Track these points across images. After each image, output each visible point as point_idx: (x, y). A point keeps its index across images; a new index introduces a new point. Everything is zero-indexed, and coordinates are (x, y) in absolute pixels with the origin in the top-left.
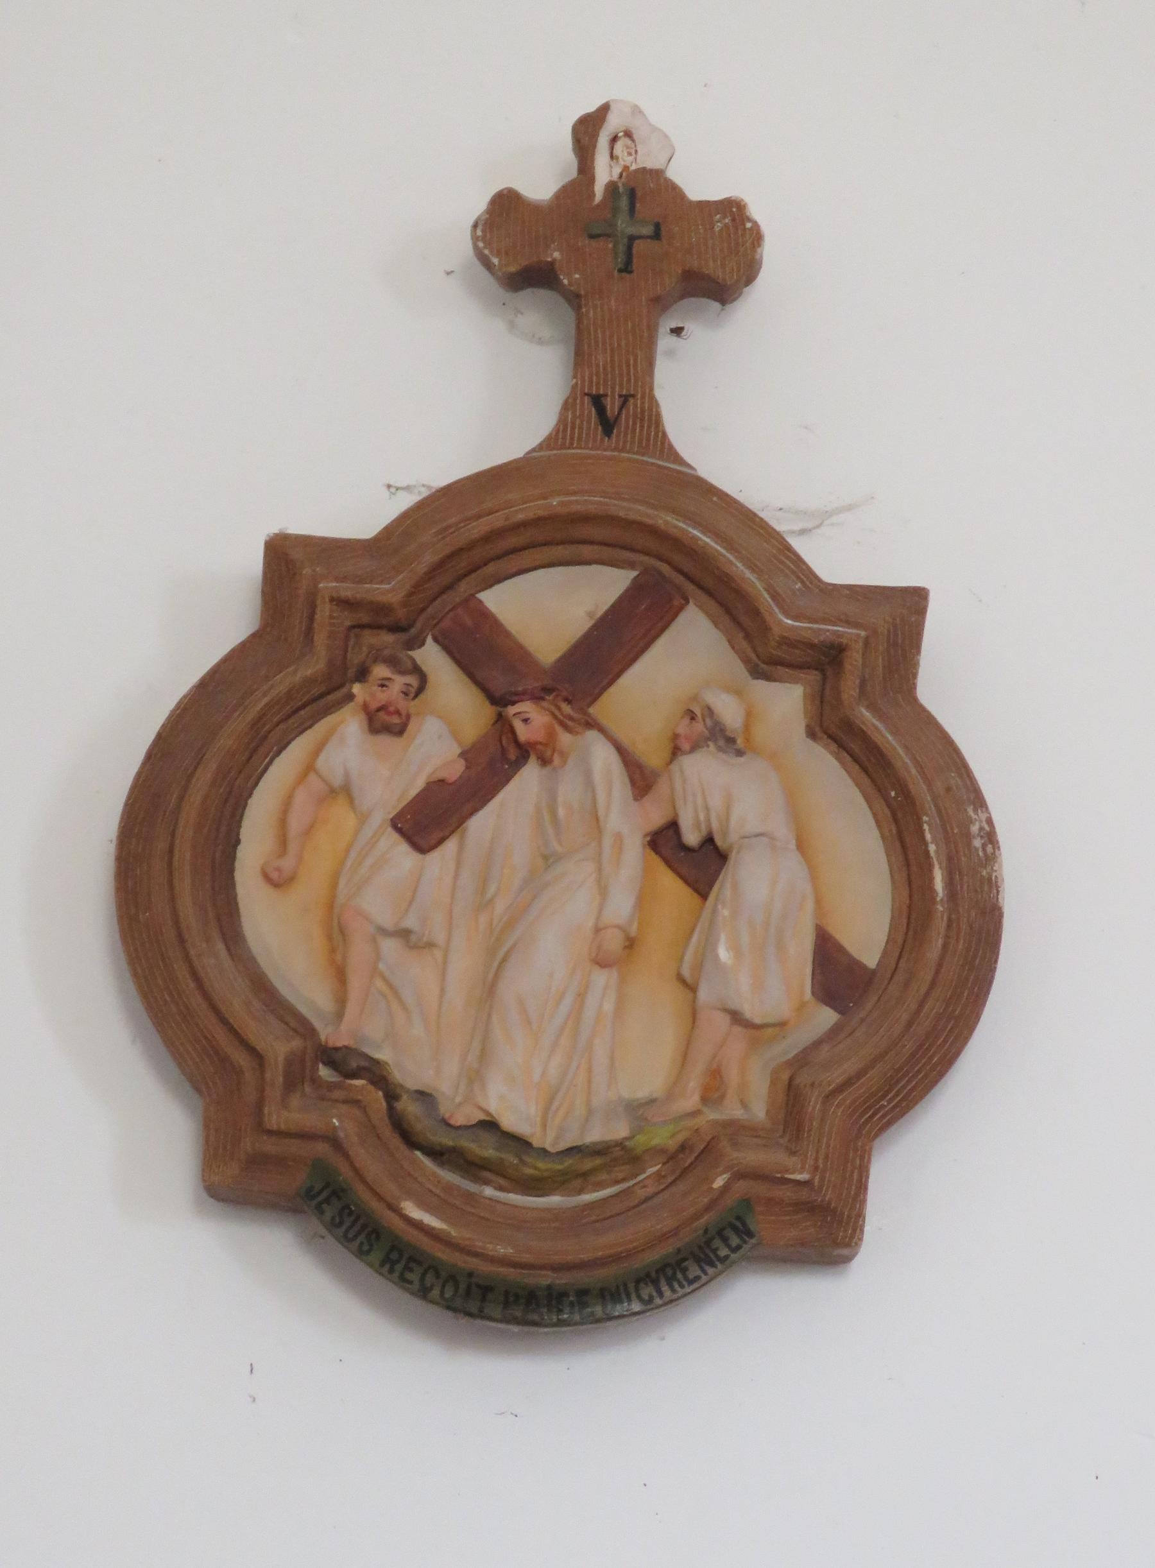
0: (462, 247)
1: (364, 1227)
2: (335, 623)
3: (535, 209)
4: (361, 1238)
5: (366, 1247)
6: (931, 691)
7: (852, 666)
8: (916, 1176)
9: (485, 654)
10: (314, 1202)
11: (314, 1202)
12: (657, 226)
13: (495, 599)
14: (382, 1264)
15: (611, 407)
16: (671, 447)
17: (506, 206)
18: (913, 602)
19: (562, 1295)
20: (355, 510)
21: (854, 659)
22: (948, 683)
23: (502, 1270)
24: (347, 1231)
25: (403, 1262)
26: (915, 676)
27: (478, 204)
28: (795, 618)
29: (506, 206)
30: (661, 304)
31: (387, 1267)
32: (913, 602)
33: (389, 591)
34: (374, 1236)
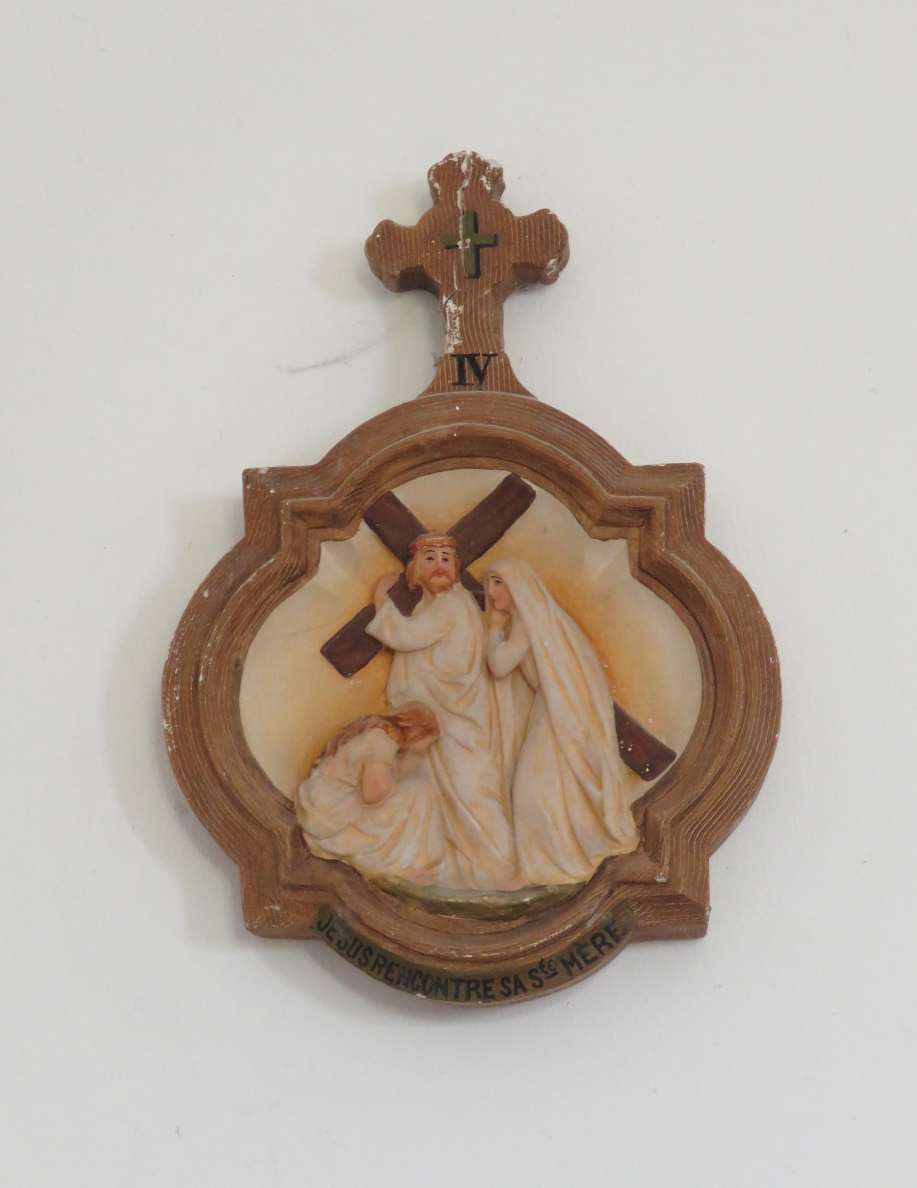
0: (361, 257)
1: (361, 945)
2: (282, 520)
3: (409, 231)
4: (360, 955)
5: (364, 960)
6: (714, 534)
7: (658, 522)
8: (737, 872)
9: (398, 532)
10: (324, 932)
11: (324, 932)
12: (496, 237)
13: (403, 494)
14: (373, 969)
15: (475, 365)
16: (518, 383)
17: (387, 230)
18: (692, 475)
19: (369, 950)
20: (303, 430)
21: (659, 517)
22: (728, 527)
23: (477, 968)
24: (349, 951)
25: (482, 986)
26: (703, 512)
27: (367, 229)
28: (613, 491)
29: (387, 230)
30: (502, 293)
31: (377, 969)
32: (692, 475)
33: (332, 500)
34: (367, 952)
